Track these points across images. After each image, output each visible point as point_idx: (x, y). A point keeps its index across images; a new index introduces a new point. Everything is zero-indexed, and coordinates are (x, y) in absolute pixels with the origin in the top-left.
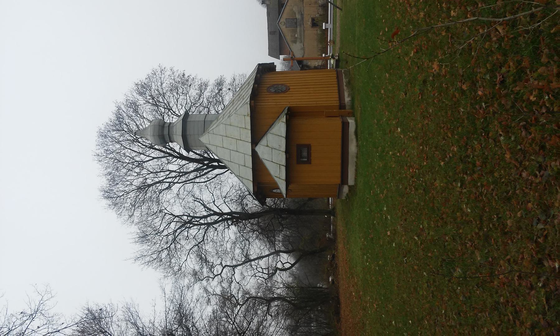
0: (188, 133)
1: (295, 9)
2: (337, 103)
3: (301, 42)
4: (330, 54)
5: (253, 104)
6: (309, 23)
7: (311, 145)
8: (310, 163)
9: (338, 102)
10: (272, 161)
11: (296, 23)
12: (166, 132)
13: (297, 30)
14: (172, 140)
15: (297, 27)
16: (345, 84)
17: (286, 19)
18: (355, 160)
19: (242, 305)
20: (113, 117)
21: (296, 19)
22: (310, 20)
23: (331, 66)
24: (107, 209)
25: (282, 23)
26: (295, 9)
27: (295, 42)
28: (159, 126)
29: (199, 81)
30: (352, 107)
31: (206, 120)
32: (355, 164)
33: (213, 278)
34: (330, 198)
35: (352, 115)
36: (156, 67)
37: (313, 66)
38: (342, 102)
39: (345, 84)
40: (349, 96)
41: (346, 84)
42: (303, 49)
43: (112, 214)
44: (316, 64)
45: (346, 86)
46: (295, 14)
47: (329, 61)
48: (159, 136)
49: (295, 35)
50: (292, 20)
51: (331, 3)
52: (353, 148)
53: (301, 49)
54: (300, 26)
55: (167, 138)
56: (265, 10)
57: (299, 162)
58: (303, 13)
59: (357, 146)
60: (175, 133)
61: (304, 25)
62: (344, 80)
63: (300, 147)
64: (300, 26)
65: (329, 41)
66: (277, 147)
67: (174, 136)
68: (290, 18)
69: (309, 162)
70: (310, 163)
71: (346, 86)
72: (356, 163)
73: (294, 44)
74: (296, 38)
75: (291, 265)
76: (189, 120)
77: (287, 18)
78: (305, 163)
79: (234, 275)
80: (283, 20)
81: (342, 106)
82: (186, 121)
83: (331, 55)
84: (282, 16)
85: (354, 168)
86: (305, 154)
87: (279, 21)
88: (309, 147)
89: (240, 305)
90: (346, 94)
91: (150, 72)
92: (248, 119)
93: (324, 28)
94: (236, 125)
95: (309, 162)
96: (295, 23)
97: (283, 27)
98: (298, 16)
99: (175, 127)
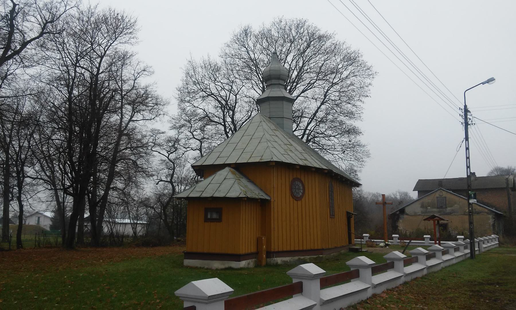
0: (272, 102)
1: (456, 206)
2: (274, 248)
3: (422, 212)
4: (390, 242)
5: (271, 164)
7: (221, 223)
8: (205, 221)
9: (276, 250)
10: (210, 184)
11: (441, 207)
13: (435, 208)
16: (302, 257)
17: (446, 197)
18: (206, 267)
19: (168, 158)
20: (322, 33)
23: (378, 243)
24: (233, 33)
26: (456, 206)
28: (280, 75)
29: (361, 112)
30: (268, 265)
31: (284, 119)
32: (202, 266)
33: (190, 132)
35: (258, 265)
36: (374, 70)
37: (398, 225)
38: (275, 255)
39: (302, 257)
40: (284, 261)
41: (302, 259)
42: (415, 215)
43: (228, 38)
44: (400, 227)
45: (299, 259)
46: (451, 206)
47: (383, 241)
48: (270, 75)
49: (429, 206)
51: (409, 243)
55: (269, 83)
56: (485, 175)
57: (207, 211)
58: (453, 214)
59: (217, 269)
60: (273, 90)
62: (308, 257)
63: (219, 211)
65: (405, 241)
66: (220, 189)
69: (206, 220)
70: (205, 221)
71: (299, 259)
72: (203, 268)
73: (420, 206)
74: (426, 208)
78: (206, 216)
79: (192, 149)
80: (444, 194)
81: (270, 254)
82: (283, 101)
83: (389, 243)
84: (448, 193)
85: (199, 266)
86: (215, 216)
87: (444, 190)
88: (219, 220)
89: (169, 156)
90: (287, 259)
91: (369, 64)
92: (257, 160)
93: (425, 236)
94: (257, 148)
95: (206, 220)
96: (442, 206)
97: (437, 194)
98: (449, 209)
99: (279, 90)
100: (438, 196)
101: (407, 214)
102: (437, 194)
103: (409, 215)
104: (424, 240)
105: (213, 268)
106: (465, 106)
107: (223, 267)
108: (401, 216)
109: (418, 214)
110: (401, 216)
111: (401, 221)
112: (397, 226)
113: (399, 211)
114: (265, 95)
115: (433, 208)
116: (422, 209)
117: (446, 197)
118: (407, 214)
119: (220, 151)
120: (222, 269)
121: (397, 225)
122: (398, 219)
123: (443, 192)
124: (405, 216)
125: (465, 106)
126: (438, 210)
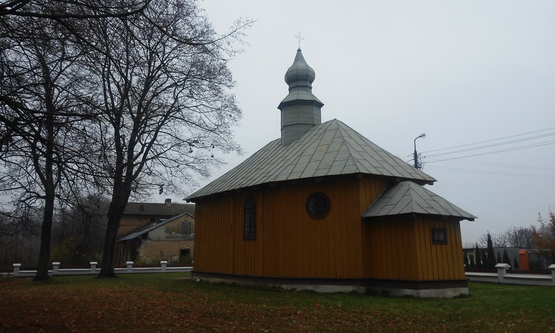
3: (167, 237)
6: (185, 247)
11: (186, 233)
12: (301, 83)
13: (179, 233)
14: (293, 89)
15: (182, 233)
17: (190, 223)
18: (441, 296)
21: (190, 233)
22: (188, 248)
25: (187, 218)
27: (167, 231)
34: (36, 271)
37: (139, 251)
42: (159, 240)
50: (189, 228)
52: (450, 293)
53: (159, 237)
54: (183, 237)
55: (294, 85)
61: (184, 241)
64: (183, 237)
67: (296, 92)
68: (191, 227)
73: (165, 230)
74: (171, 233)
75: (125, 212)
76: (314, 108)
77: (191, 224)
85: (434, 296)
93: (14, 265)
96: (186, 232)
97: (182, 220)
100: (183, 221)
101: (150, 239)
102: (182, 220)
103: (152, 240)
104: (126, 268)
105: (447, 297)
106: (415, 152)
107: (457, 294)
108: (143, 241)
109: (162, 239)
110: (143, 241)
111: (142, 246)
112: (138, 253)
113: (141, 236)
114: (294, 98)
115: (177, 233)
116: (166, 234)
117: (190, 223)
118: (150, 239)
119: (337, 162)
120: (455, 298)
121: (137, 251)
122: (139, 245)
123: (189, 217)
124: (148, 241)
125: (415, 152)
126: (182, 235)
